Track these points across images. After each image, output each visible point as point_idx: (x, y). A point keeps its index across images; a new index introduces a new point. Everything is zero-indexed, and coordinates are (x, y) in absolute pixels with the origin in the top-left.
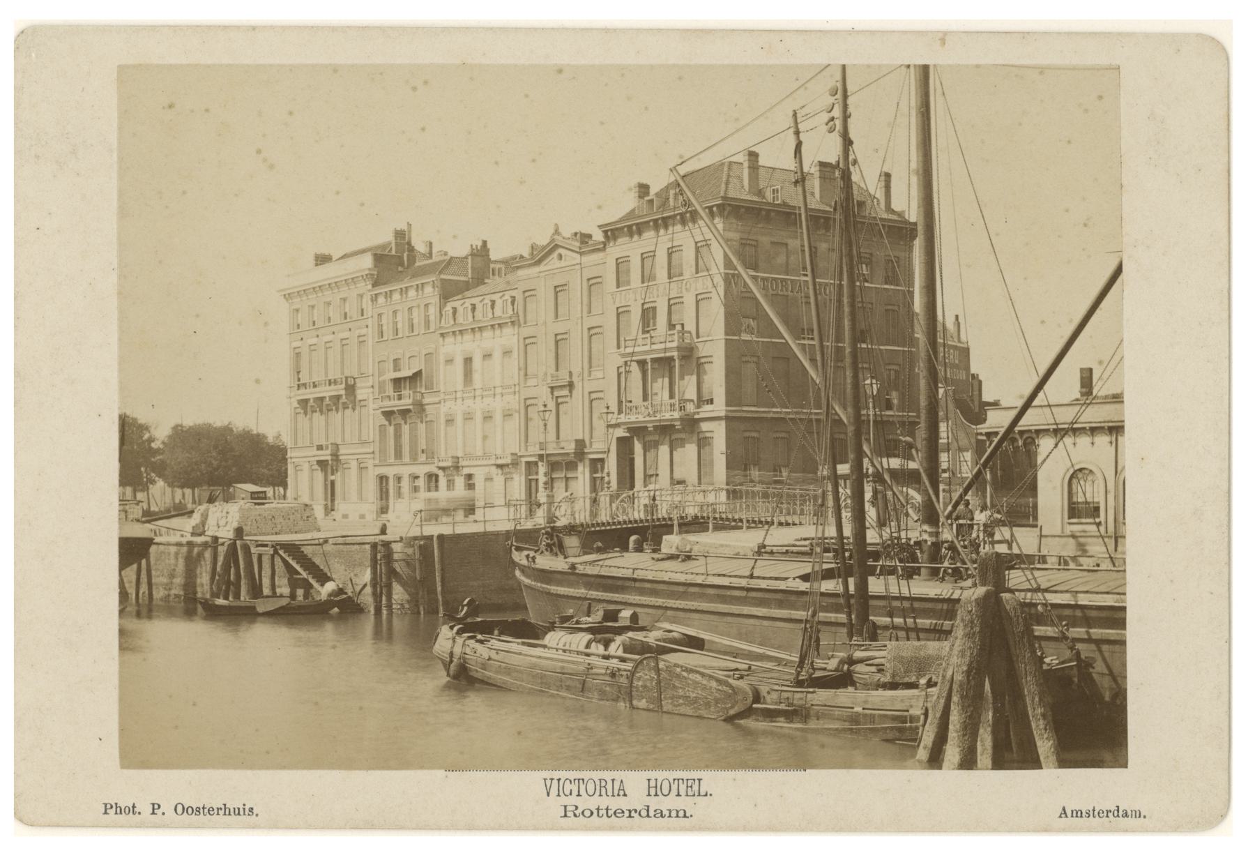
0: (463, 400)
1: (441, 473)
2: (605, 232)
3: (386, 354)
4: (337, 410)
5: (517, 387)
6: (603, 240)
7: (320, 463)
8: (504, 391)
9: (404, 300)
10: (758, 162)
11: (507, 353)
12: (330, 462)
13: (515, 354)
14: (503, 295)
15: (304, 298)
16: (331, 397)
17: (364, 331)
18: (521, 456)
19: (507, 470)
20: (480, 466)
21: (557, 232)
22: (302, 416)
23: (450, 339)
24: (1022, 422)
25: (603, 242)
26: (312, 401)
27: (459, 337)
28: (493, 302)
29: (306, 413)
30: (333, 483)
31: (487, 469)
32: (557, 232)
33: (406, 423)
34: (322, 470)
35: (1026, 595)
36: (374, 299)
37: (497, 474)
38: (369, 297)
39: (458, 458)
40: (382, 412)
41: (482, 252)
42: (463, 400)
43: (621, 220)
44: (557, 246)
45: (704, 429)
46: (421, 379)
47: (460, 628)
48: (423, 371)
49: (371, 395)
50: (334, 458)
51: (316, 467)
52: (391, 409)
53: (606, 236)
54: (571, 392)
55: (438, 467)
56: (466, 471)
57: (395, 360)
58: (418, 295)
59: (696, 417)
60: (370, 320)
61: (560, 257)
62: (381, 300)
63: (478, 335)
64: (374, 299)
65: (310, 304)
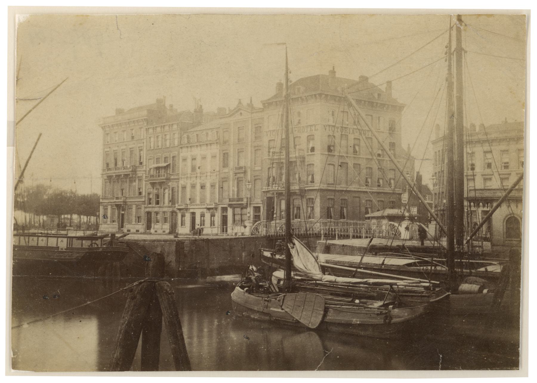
0: (210, 177)
1: (178, 211)
2: (264, 104)
3: (160, 155)
4: (118, 182)
5: (218, 172)
6: (262, 107)
7: (117, 205)
8: (192, 176)
9: (171, 130)
10: (335, 75)
11: (214, 157)
12: (122, 205)
13: (218, 158)
14: (202, 132)
15: (120, 127)
16: (116, 176)
17: (142, 145)
18: (219, 204)
19: (211, 211)
20: (196, 208)
21: (240, 103)
22: (108, 183)
23: (184, 150)
24: (511, 194)
25: (262, 109)
26: (122, 176)
27: (209, 147)
28: (207, 133)
29: (110, 182)
30: (123, 215)
31: (202, 210)
32: (240, 103)
33: (161, 188)
34: (117, 209)
35: (431, 268)
36: (147, 130)
37: (207, 213)
38: (145, 129)
39: (188, 205)
40: (150, 183)
41: (199, 111)
42: (210, 177)
43: (272, 98)
44: (240, 109)
45: (466, 196)
46: (170, 168)
47: (247, 290)
48: (171, 165)
49: (144, 175)
50: (124, 203)
51: (115, 207)
52: (155, 181)
53: (265, 107)
54: (244, 175)
55: (177, 209)
56: (192, 211)
57: (165, 158)
58: (161, 130)
59: (306, 189)
60: (145, 140)
61: (241, 114)
62: (151, 131)
63: (189, 149)
64: (147, 130)
65: (114, 131)
